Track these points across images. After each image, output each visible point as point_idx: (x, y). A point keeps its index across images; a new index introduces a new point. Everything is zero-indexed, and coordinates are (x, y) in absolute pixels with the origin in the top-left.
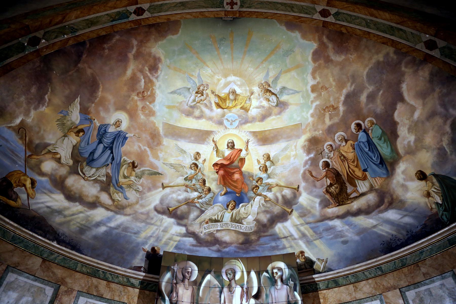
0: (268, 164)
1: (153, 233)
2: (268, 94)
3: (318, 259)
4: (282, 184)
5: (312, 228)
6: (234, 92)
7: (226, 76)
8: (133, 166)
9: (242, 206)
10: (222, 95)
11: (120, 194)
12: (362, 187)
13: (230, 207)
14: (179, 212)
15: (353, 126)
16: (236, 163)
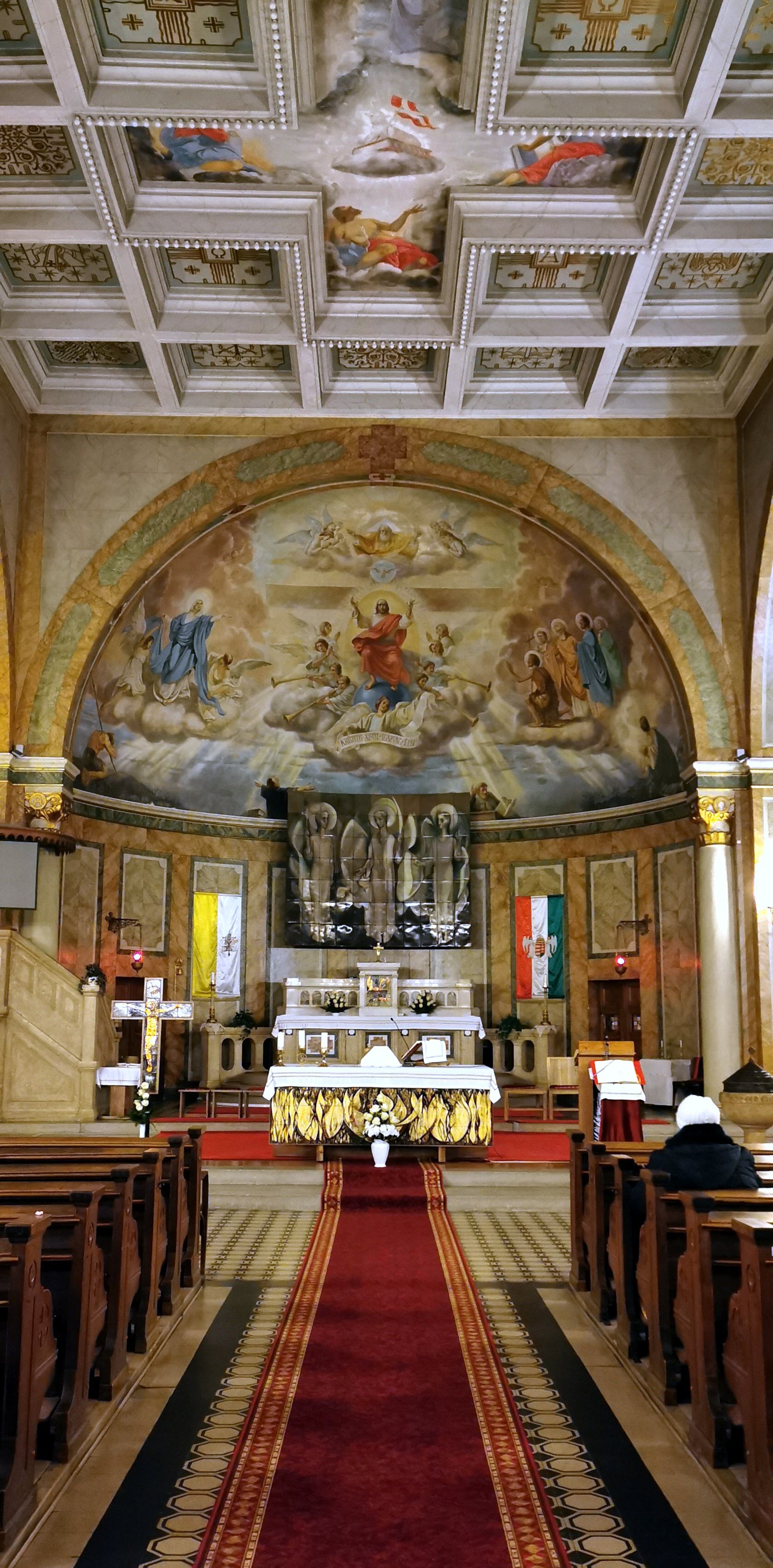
0: (444, 641)
1: (267, 757)
2: (447, 538)
3: (504, 798)
4: (465, 676)
5: (502, 752)
6: (388, 531)
7: (373, 510)
8: (226, 661)
9: (400, 707)
10: (367, 535)
11: (213, 710)
12: (579, 709)
13: (381, 708)
14: (301, 720)
15: (578, 618)
16: (391, 637)
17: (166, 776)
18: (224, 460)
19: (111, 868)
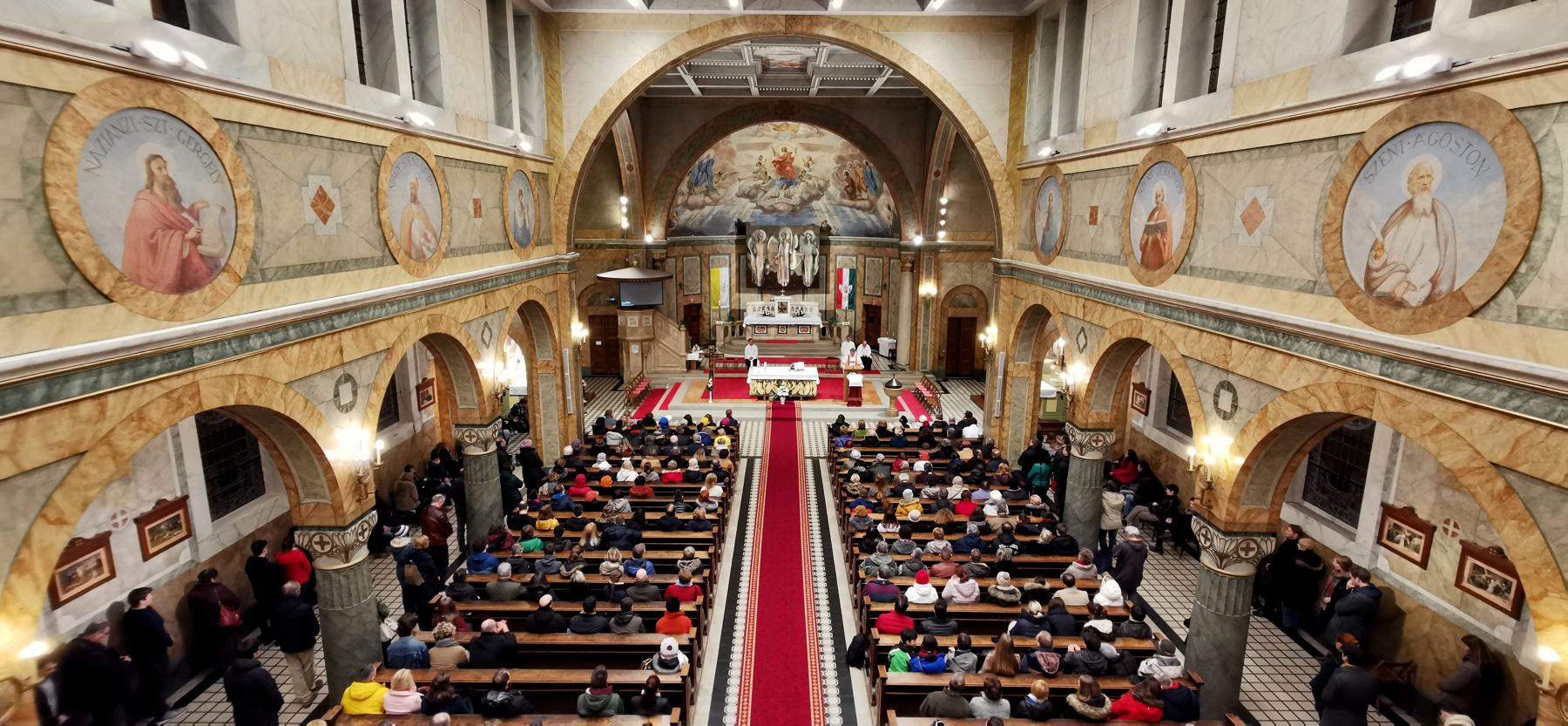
8: (720, 174)
17: (697, 223)
18: (720, 116)
19: (679, 264)
